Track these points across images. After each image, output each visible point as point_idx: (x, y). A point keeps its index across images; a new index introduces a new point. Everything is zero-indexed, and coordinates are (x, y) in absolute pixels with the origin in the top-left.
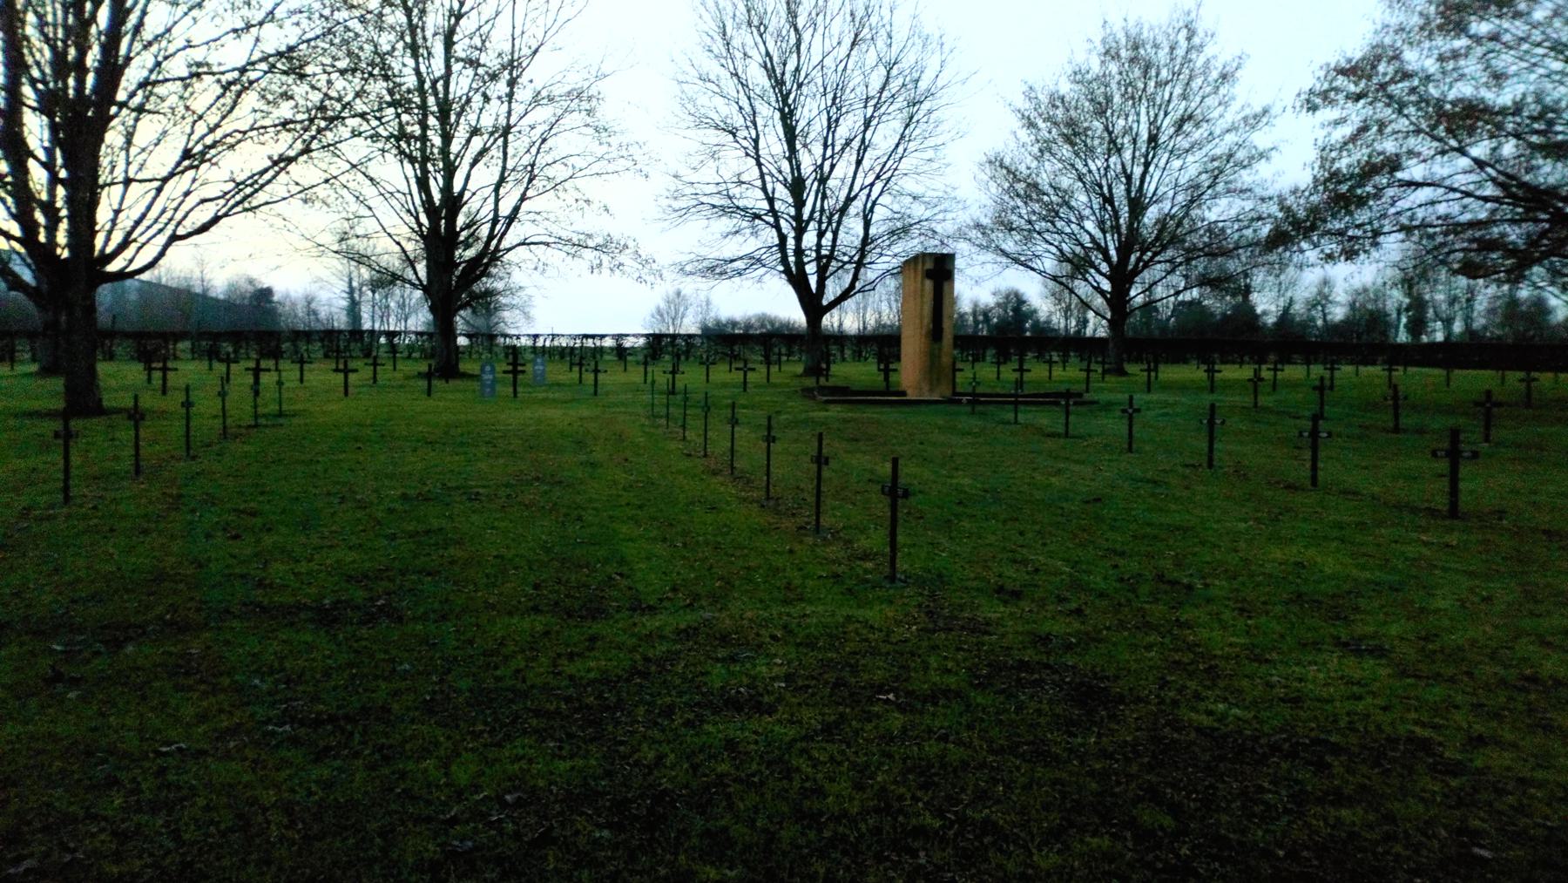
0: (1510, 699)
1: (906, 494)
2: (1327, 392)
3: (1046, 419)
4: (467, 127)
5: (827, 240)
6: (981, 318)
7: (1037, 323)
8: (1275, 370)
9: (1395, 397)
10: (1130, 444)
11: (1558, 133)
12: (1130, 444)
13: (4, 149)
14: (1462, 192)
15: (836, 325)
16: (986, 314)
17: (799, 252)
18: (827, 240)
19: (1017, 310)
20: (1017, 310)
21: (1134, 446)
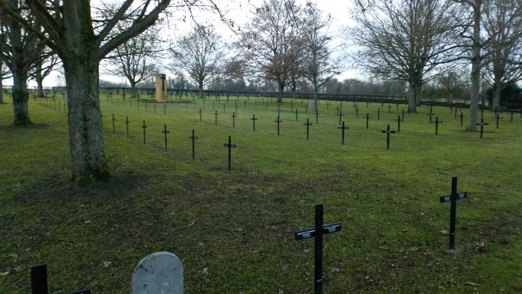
0: (216, 192)
1: (129, 122)
2: (329, 105)
3: (184, 105)
4: (194, 25)
5: (135, 67)
6: (171, 82)
7: (188, 84)
8: (180, 97)
9: (292, 106)
10: (317, 122)
11: (498, 39)
12: (317, 122)
13: (126, 1)
14: (435, 54)
15: (124, 83)
16: (173, 81)
17: (129, 70)
18: (135, 67)
19: (182, 80)
20: (182, 80)
21: (318, 122)
